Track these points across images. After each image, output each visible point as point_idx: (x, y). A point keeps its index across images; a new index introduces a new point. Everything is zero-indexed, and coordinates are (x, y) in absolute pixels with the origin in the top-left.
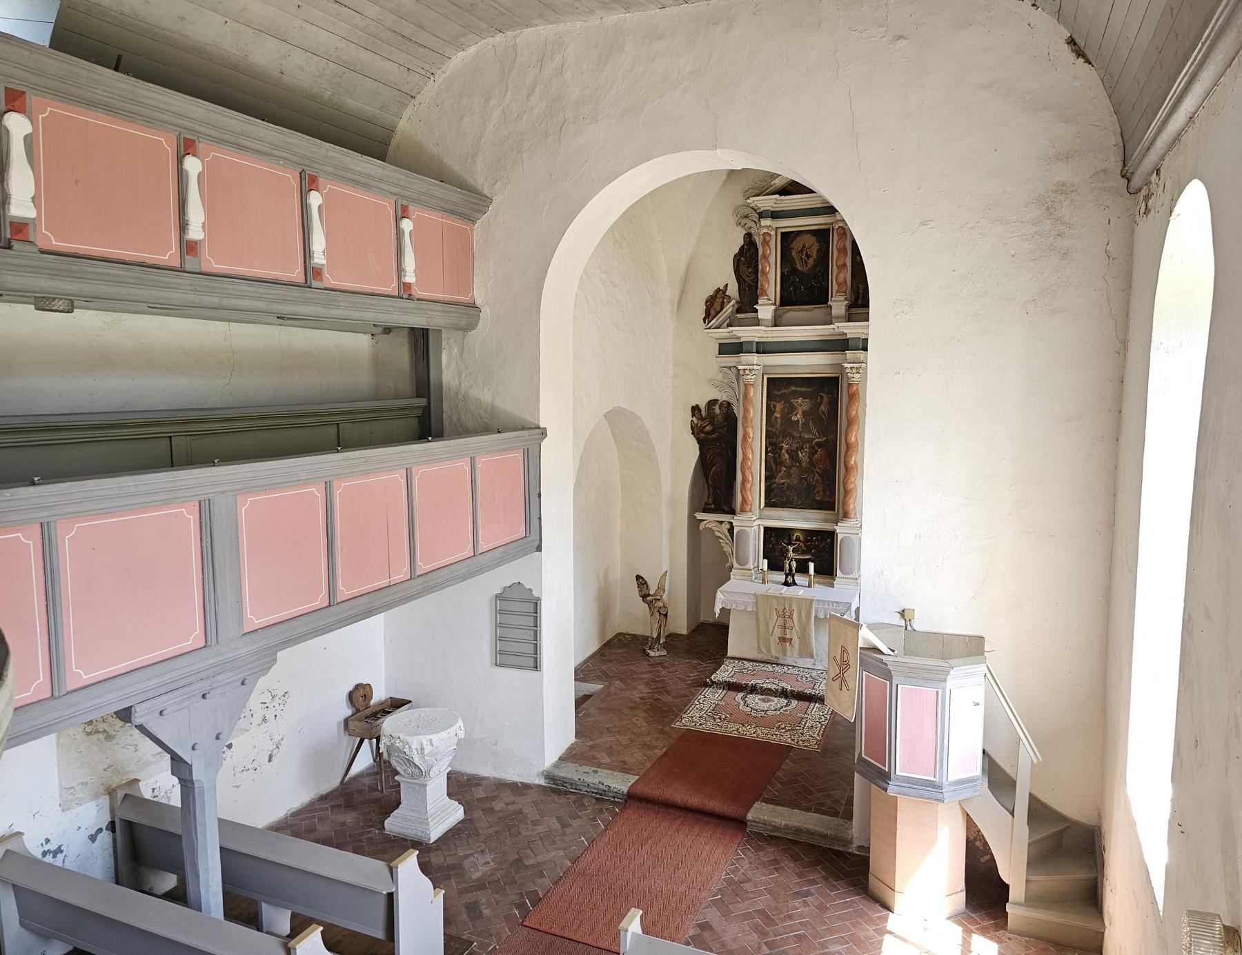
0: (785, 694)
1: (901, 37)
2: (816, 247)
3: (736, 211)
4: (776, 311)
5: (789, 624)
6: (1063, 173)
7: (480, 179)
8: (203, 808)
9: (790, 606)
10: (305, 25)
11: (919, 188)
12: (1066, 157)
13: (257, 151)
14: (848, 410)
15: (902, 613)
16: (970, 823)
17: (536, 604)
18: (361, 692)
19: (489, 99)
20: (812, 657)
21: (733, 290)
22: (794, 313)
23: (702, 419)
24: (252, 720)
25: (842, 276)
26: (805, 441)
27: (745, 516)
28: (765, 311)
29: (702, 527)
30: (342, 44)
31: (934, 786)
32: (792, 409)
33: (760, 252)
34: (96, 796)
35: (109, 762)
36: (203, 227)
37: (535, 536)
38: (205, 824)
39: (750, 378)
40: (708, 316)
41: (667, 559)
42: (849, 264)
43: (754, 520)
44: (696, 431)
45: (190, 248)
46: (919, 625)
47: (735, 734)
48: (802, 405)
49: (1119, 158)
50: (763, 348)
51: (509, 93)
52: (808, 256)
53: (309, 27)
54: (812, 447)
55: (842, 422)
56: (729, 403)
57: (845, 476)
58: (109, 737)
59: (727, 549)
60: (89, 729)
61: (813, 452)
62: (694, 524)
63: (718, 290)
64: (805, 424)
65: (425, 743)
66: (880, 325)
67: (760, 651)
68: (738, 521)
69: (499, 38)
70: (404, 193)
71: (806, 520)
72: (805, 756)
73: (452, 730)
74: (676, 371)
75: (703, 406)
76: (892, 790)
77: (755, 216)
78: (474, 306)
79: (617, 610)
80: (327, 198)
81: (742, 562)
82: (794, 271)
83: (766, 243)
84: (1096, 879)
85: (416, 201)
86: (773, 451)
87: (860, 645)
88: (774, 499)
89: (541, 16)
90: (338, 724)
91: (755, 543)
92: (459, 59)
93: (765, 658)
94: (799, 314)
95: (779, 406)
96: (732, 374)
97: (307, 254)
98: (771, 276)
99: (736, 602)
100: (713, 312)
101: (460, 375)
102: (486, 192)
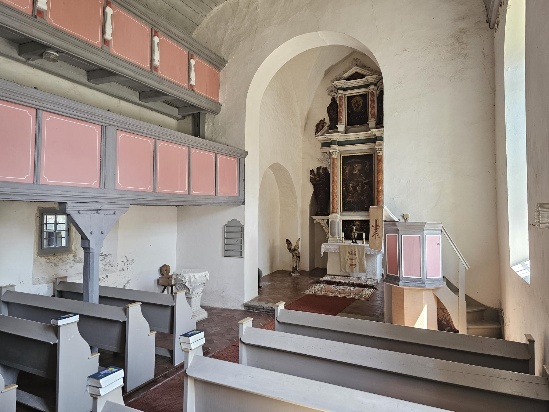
0: (353, 285)
2: (361, 102)
3: (328, 89)
4: (345, 127)
6: (462, 25)
7: (223, 54)
8: (93, 262)
13: (134, 13)
15: (403, 216)
16: (438, 301)
17: (242, 227)
18: (165, 268)
19: (227, 23)
20: (365, 272)
21: (327, 120)
22: (353, 128)
23: (314, 175)
24: (118, 268)
25: (373, 111)
26: (359, 182)
27: (334, 214)
28: (341, 127)
29: (315, 222)
31: (420, 281)
32: (354, 169)
34: (48, 283)
35: (55, 273)
36: (112, 35)
38: (93, 269)
39: (335, 156)
40: (317, 132)
41: (300, 234)
42: (376, 107)
43: (338, 217)
44: (312, 181)
45: (106, 42)
46: (410, 220)
47: (330, 295)
48: (358, 167)
49: (485, 16)
52: (359, 105)
54: (362, 184)
55: (375, 172)
56: (326, 168)
58: (56, 265)
59: (326, 231)
60: (48, 261)
61: (363, 186)
62: (312, 221)
64: (359, 175)
65: (191, 276)
66: (387, 131)
67: (341, 271)
68: (330, 217)
70: (192, 48)
71: (360, 216)
72: (363, 301)
74: (302, 156)
75: (315, 170)
78: (219, 103)
79: (278, 259)
80: (161, 41)
81: (333, 235)
82: (353, 112)
83: (340, 100)
86: (346, 187)
88: (347, 208)
90: (155, 281)
91: (338, 227)
92: (216, 9)
93: (344, 275)
94: (355, 129)
95: (348, 168)
97: (152, 60)
98: (343, 113)
99: (330, 249)
100: (319, 130)
101: (212, 133)
102: (225, 58)
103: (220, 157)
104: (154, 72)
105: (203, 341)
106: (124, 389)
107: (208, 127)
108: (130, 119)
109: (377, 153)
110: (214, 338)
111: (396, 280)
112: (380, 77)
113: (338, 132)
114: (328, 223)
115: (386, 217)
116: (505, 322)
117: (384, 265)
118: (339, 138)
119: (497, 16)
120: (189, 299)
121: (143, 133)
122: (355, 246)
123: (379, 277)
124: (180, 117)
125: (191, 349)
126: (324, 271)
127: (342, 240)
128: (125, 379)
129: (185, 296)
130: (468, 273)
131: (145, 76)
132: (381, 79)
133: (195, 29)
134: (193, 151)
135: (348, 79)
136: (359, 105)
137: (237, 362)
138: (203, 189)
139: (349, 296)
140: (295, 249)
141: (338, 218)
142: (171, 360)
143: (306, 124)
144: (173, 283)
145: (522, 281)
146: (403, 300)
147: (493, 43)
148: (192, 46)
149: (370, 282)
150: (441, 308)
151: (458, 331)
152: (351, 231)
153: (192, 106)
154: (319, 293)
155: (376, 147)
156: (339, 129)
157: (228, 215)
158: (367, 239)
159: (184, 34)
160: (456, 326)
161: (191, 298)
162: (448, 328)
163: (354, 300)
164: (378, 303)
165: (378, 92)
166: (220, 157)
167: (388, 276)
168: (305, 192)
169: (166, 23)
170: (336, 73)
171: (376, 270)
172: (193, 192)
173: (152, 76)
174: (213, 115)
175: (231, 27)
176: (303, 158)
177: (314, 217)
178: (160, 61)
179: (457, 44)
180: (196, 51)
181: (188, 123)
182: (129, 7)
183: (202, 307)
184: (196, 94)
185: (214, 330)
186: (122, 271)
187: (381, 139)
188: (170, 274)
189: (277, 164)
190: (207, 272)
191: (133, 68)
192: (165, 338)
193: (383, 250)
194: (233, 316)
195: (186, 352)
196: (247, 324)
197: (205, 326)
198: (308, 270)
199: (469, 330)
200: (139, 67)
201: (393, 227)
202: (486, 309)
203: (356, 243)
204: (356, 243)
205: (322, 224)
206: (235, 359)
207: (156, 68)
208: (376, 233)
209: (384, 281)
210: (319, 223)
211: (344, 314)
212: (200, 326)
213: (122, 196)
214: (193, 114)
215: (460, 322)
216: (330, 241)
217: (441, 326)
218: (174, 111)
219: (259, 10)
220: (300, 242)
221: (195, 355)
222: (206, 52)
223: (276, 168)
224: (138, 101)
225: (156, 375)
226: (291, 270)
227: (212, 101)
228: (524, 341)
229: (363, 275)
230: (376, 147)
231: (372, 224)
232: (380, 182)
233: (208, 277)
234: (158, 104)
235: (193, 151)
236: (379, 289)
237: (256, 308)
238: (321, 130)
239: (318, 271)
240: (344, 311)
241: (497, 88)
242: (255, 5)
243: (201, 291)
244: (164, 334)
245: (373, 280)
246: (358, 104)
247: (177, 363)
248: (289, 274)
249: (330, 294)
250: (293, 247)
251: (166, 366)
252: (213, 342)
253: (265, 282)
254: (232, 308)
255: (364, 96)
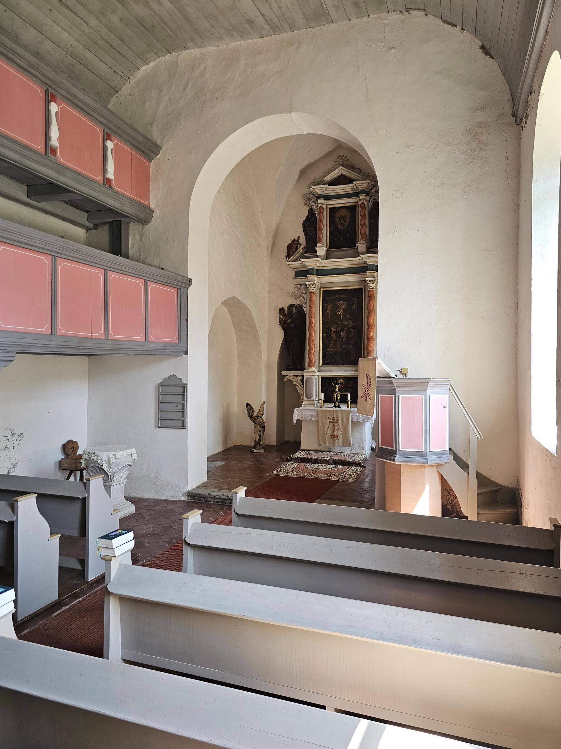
0: (334, 462)
1: (392, 48)
2: (348, 217)
3: (304, 197)
5: (336, 426)
6: (482, 117)
7: (156, 136)
9: (337, 416)
10: (53, 24)
11: (405, 128)
12: (481, 108)
14: (368, 305)
15: (401, 371)
16: (443, 481)
17: (184, 387)
18: (71, 445)
19: (161, 91)
20: (350, 445)
21: (303, 240)
23: (285, 315)
25: (363, 230)
28: (321, 250)
29: (285, 379)
30: (75, 44)
31: (422, 455)
32: (337, 308)
33: (318, 218)
37: (183, 344)
40: (288, 255)
41: (264, 394)
42: (367, 224)
43: (316, 373)
44: (282, 323)
47: (305, 476)
49: (511, 107)
50: (321, 273)
51: (173, 87)
52: (345, 221)
53: (56, 27)
57: (368, 343)
59: (300, 391)
62: (281, 378)
63: (294, 240)
65: (111, 456)
66: (385, 256)
67: (319, 444)
68: (305, 373)
69: (168, 57)
70: (109, 125)
71: (345, 371)
72: (347, 484)
73: (129, 452)
74: (267, 291)
75: (286, 309)
76: (397, 460)
77: (314, 199)
78: (149, 208)
79: (235, 430)
81: (309, 396)
83: (321, 212)
84: (518, 513)
85: (116, 133)
87: (377, 375)
88: (327, 360)
89: (192, 39)
90: (55, 463)
91: (316, 386)
92: (145, 69)
93: (323, 449)
94: (340, 253)
96: (302, 289)
97: (47, 138)
98: (324, 231)
100: (291, 253)
101: (140, 251)
102: (158, 143)
103: (151, 286)
104: (51, 156)
105: (132, 545)
106: (14, 616)
107: (133, 241)
108: (15, 225)
109: (368, 287)
110: (145, 540)
111: (392, 454)
112: (373, 183)
113: (317, 257)
114: (302, 380)
115: (379, 371)
116: (523, 505)
117: (374, 436)
118: (318, 265)
119: (526, 108)
120: (108, 488)
121: (35, 246)
122: (337, 411)
123: (367, 451)
124: (91, 225)
125: (115, 555)
126: (296, 446)
127: (321, 404)
128: (15, 602)
129: (102, 484)
130: (480, 443)
131: (38, 162)
132: (376, 185)
133: (113, 96)
134: (112, 276)
135: (331, 183)
136: (345, 221)
137: (180, 570)
138: (128, 333)
139: (330, 478)
140: (258, 416)
141: (316, 374)
142: (83, 573)
143: (274, 244)
144: (83, 466)
145: (546, 452)
146: (399, 481)
147: (520, 145)
148: (108, 120)
149: (357, 458)
150: (446, 490)
151: (467, 518)
152: (333, 391)
153: (108, 210)
154: (290, 474)
155: (367, 279)
156: (319, 253)
157: (164, 370)
158: (354, 401)
159: (96, 101)
160: (465, 511)
161: (110, 486)
162: (455, 514)
163: (336, 482)
164: (366, 485)
165: (371, 204)
166: (151, 286)
167: (380, 449)
168: (271, 339)
169: (69, 85)
170: (316, 174)
171: (364, 441)
172: (113, 335)
173: (47, 162)
174: (140, 225)
175: (167, 97)
176: (270, 292)
177: (284, 373)
178: (60, 140)
179: (475, 143)
180: (115, 129)
181: (103, 234)
182: (10, 55)
183: (127, 498)
184: (116, 192)
185: (144, 530)
186: (5, 452)
187: (375, 268)
188: (78, 453)
189: (233, 298)
190: (134, 450)
191: (18, 148)
192: (74, 544)
193: (375, 416)
194: (172, 510)
195: (108, 560)
196: (194, 517)
197: (132, 524)
198: (275, 444)
199: (481, 517)
200: (26, 147)
201: (387, 385)
202: (500, 489)
203: (339, 407)
204: (339, 407)
205: (295, 383)
206: (177, 565)
207: (53, 151)
208: (366, 394)
209: (376, 456)
210: (291, 381)
211: (323, 501)
212: (125, 525)
213: (5, 340)
214: (111, 223)
215: (469, 508)
216: (306, 406)
217: (446, 511)
218: (82, 217)
219: (207, 76)
220: (265, 406)
221: (120, 564)
222: (130, 131)
223: (233, 305)
224: (24, 198)
225: (60, 595)
226: (253, 444)
227: (140, 204)
228: (548, 526)
229: (347, 449)
230: (367, 279)
231: (362, 381)
232: (371, 327)
233: (135, 457)
234: (57, 206)
235: (112, 276)
236: (368, 466)
237: (204, 498)
238: (294, 253)
239: (288, 446)
240: (323, 497)
241: (523, 204)
242: (202, 67)
243: (125, 476)
244: (71, 537)
245: (360, 456)
246: (343, 217)
247: (91, 577)
248: (249, 450)
249: (304, 475)
250: (255, 413)
251: (75, 582)
252: (144, 546)
253: (217, 461)
254: (169, 498)
255: (352, 209)
